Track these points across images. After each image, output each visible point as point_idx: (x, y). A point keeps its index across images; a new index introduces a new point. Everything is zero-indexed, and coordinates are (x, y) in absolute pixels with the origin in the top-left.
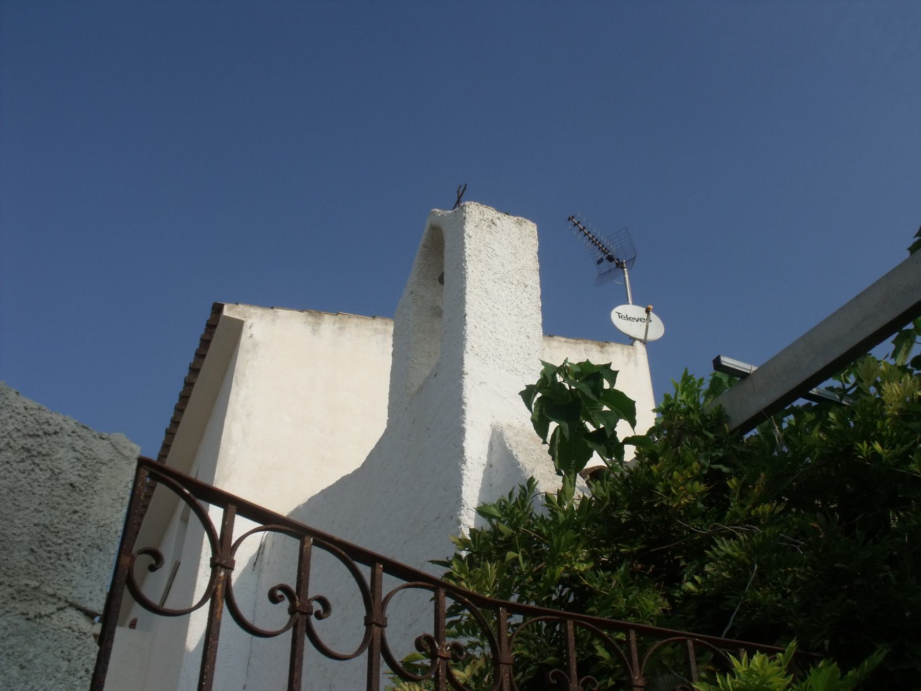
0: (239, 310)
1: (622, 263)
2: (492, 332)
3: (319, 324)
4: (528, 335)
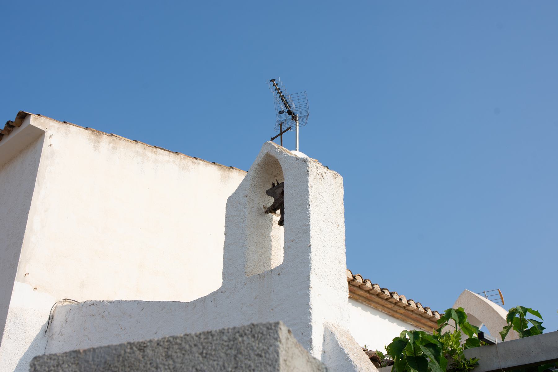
0: (41, 121)
1: (296, 116)
2: (323, 259)
3: (99, 142)
4: (340, 261)
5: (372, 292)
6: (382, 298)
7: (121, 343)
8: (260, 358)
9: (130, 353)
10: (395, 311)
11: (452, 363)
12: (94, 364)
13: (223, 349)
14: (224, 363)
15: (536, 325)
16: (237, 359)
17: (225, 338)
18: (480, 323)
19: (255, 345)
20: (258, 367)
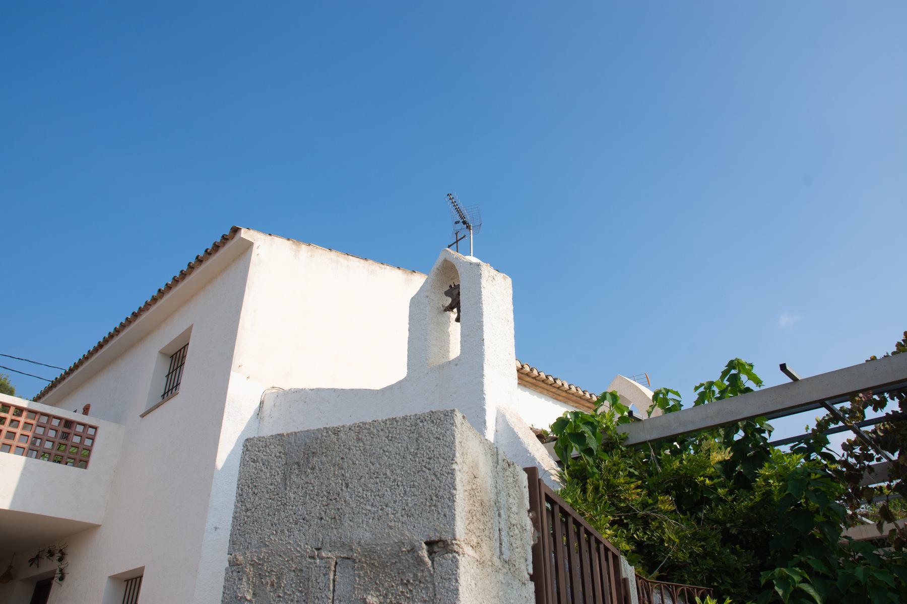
1: (470, 226)
3: (299, 251)
5: (538, 378)
6: (547, 384)
7: (318, 428)
8: (439, 441)
9: (326, 437)
10: (558, 395)
11: (606, 438)
12: (296, 446)
13: (406, 433)
14: (407, 445)
15: (677, 403)
16: (419, 441)
17: (408, 424)
18: (630, 402)
19: (434, 430)
20: (436, 448)
